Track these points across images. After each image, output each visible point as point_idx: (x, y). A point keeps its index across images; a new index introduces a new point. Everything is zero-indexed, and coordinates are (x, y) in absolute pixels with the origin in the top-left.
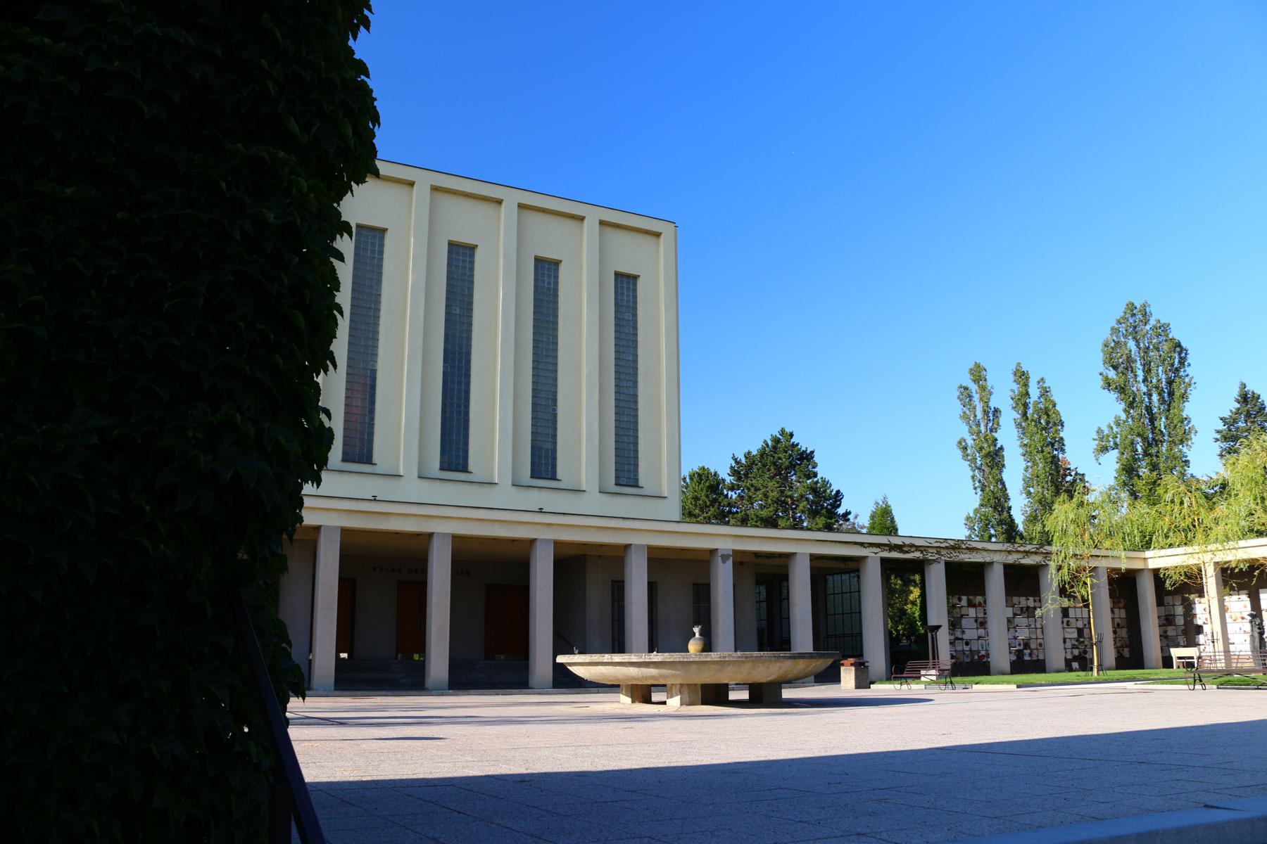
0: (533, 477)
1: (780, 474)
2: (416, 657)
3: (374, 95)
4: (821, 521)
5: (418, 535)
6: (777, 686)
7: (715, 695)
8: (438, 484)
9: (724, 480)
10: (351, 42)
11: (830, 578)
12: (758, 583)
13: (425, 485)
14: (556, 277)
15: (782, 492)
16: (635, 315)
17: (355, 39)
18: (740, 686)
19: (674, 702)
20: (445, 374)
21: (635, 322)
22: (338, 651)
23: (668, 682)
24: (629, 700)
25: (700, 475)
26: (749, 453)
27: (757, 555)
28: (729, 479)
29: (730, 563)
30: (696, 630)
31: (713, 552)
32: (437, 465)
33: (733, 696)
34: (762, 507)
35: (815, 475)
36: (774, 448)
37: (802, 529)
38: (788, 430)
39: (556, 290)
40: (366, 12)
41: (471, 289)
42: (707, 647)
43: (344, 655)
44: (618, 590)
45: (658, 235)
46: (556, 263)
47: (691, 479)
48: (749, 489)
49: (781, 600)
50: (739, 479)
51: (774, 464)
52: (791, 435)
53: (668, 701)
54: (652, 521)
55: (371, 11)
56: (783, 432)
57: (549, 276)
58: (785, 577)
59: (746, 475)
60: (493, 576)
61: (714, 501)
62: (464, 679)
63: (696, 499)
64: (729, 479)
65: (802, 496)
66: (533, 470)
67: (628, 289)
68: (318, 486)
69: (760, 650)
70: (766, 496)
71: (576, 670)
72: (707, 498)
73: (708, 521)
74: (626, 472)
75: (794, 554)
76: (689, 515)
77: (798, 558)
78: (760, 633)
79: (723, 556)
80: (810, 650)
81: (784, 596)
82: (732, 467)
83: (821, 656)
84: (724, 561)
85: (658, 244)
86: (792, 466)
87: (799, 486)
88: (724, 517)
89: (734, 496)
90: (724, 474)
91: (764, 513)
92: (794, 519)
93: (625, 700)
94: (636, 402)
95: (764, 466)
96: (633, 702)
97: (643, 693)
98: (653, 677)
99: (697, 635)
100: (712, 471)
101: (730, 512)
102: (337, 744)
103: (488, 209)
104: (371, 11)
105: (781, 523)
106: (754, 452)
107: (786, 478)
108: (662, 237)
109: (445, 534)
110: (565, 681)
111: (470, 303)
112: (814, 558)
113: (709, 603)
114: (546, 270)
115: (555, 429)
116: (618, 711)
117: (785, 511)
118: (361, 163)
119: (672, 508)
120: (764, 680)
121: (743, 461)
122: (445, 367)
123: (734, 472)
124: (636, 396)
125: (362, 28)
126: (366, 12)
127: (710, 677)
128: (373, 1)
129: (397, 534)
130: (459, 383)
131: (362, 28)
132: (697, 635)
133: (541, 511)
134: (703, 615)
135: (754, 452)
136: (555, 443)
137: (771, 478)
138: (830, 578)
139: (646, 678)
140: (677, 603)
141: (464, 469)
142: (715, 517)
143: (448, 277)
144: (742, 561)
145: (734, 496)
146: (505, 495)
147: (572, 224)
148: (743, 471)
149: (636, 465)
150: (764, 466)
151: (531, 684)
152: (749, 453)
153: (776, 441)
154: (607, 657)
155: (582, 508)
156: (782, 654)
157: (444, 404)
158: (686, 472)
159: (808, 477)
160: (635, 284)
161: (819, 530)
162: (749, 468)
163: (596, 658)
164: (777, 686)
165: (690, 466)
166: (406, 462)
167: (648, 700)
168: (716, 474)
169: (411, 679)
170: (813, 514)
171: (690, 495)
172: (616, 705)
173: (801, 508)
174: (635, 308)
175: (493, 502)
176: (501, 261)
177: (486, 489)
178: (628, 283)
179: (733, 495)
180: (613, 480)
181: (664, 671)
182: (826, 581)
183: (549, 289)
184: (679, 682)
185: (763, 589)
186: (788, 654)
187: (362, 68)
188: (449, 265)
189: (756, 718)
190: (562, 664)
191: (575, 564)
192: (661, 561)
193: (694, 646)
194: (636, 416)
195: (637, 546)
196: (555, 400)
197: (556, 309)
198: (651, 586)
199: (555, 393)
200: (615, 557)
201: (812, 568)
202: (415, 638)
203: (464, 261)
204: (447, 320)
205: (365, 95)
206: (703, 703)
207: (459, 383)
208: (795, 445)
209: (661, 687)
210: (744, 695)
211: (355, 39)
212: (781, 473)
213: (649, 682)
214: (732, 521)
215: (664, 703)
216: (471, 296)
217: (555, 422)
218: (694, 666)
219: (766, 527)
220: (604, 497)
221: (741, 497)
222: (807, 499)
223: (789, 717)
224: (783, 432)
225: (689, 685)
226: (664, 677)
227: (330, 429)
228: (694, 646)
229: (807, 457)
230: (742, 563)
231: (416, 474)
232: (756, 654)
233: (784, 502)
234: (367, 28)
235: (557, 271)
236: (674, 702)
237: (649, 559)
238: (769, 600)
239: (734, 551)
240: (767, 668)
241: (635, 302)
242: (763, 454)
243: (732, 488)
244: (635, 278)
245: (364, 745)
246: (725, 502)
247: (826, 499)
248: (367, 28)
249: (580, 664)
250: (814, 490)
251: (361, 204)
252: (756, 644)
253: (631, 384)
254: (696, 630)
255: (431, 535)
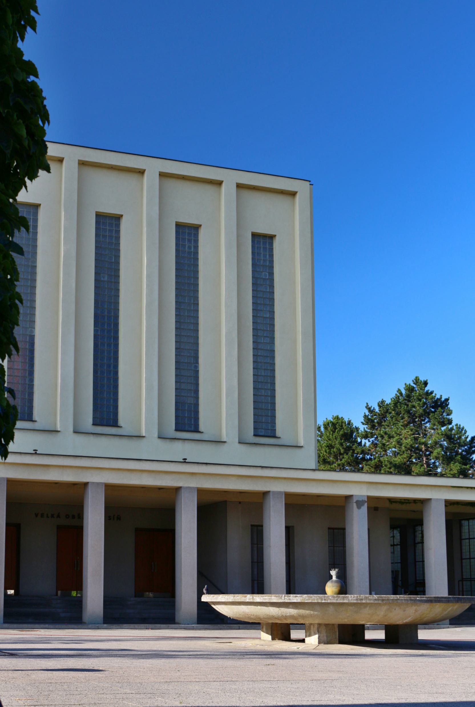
0: (177, 430)
1: (414, 422)
2: (74, 593)
3: (44, 94)
4: (455, 467)
5: (74, 484)
6: (412, 628)
7: (351, 634)
8: (92, 438)
9: (357, 429)
10: (20, 44)
11: (465, 523)
12: (393, 527)
13: (80, 439)
14: (196, 241)
15: (416, 439)
16: (272, 274)
17: (22, 40)
18: (375, 627)
19: (313, 640)
20: (96, 337)
21: (272, 280)
22: (6, 588)
23: (307, 622)
24: (269, 637)
25: (334, 424)
26: (383, 402)
27: (391, 501)
28: (362, 428)
29: (365, 509)
30: (333, 573)
31: (348, 498)
32: (90, 420)
33: (369, 635)
34: (395, 454)
35: (450, 422)
36: (408, 396)
37: (436, 475)
38: (422, 379)
39: (196, 253)
40: (33, 13)
41: (118, 257)
42: (343, 590)
43: (11, 592)
44: (257, 534)
45: (293, 194)
46: (196, 228)
47: (326, 428)
48: (382, 437)
49: (415, 544)
50: (373, 427)
51: (408, 412)
52: (426, 383)
53: (307, 640)
54: (293, 470)
55: (37, 13)
56: (417, 381)
57: (190, 241)
58: (420, 522)
59: (380, 424)
60: (143, 524)
61: (348, 449)
62: (115, 615)
63: (330, 447)
64: (362, 428)
65: (436, 443)
66: (177, 424)
67: (265, 249)
68: (5, 459)
69: (395, 593)
70: (399, 443)
71: (221, 609)
72: (341, 446)
73: (342, 469)
74: (264, 424)
75: (429, 500)
76: (324, 463)
77: (433, 504)
78: (395, 575)
79: (357, 502)
80: (446, 595)
81: (418, 539)
82: (365, 416)
83: (458, 600)
84: (359, 507)
85: (294, 204)
86: (426, 414)
87: (433, 434)
88: (358, 463)
89: (368, 444)
90: (358, 422)
91: (398, 460)
92: (428, 465)
93: (266, 637)
94: (273, 358)
95: (398, 414)
96: (273, 639)
97: (282, 631)
98: (292, 617)
99: (334, 578)
100: (346, 420)
101: (363, 459)
102: (11, 674)
103: (131, 180)
104: (37, 13)
105: (415, 469)
106: (388, 401)
107: (420, 426)
108: (298, 196)
109: (98, 484)
110: (209, 617)
111: (117, 270)
112: (449, 503)
113: (344, 546)
114: (187, 235)
115: (197, 385)
116: (259, 648)
117: (419, 458)
118: (35, 160)
119: (308, 457)
120: (400, 622)
121: (377, 410)
122: (95, 330)
123: (368, 421)
124: (273, 351)
125: (29, 29)
126: (33, 13)
127: (347, 618)
128: (39, 3)
129: (56, 483)
130: (109, 345)
131: (29, 29)
132: (334, 578)
133: (185, 461)
134: (338, 557)
135: (388, 401)
136: (197, 398)
137: (405, 426)
138: (465, 523)
139: (286, 617)
140: (314, 545)
141: (115, 424)
142: (349, 464)
143: (97, 248)
144: (377, 507)
145: (368, 444)
146: (152, 447)
147: (210, 189)
148: (376, 419)
149: (274, 417)
150: (398, 414)
151: (177, 620)
152: (383, 402)
153: (410, 389)
154: (249, 598)
155: (223, 459)
156: (418, 597)
157: (95, 365)
158: (320, 422)
159: (443, 424)
160: (271, 244)
161: (454, 476)
162: (383, 416)
163: (239, 598)
164: (412, 628)
165: (324, 416)
166: (63, 421)
167: (287, 638)
168: (349, 423)
169: (72, 615)
170: (448, 460)
171: (324, 444)
172: (257, 642)
173: (435, 454)
174: (272, 267)
175: (142, 455)
176: (145, 229)
177: (297, 451)
178: (265, 243)
179: (367, 443)
180: (252, 432)
181: (302, 612)
182: (461, 526)
183: (189, 253)
184: (317, 621)
185: (397, 534)
186: (424, 598)
187: (30, 68)
188: (97, 235)
189: (393, 659)
190: (207, 604)
191: (213, 509)
192: (298, 507)
193: (331, 588)
194: (274, 370)
195: (273, 492)
196: (196, 358)
197: (196, 272)
198: (289, 530)
199: (197, 351)
200: (254, 504)
201: (447, 514)
202: (72, 574)
203: (111, 231)
204: (96, 287)
205: (34, 94)
206: (341, 642)
207: (109, 345)
208: (429, 394)
209: (300, 626)
210: (381, 635)
211: (22, 40)
212: (415, 420)
213: (289, 621)
214: (366, 468)
215: (303, 641)
216: (118, 263)
217: (197, 378)
218: (331, 608)
219: (399, 473)
220: (243, 447)
221: (375, 445)
222: (441, 446)
223: (425, 659)
224: (417, 381)
225: (326, 625)
226: (303, 617)
227: (14, 408)
228: (331, 588)
229: (442, 405)
230: (376, 509)
231: (71, 430)
232: (392, 597)
233: (417, 449)
234: (34, 29)
235: (196, 235)
236: (313, 640)
237: (286, 505)
238: (403, 544)
239: (368, 497)
240: (403, 610)
241: (272, 262)
242: (396, 402)
243: (366, 436)
244: (272, 237)
245: (35, 675)
246: (359, 450)
247: (460, 446)
248: (34, 29)
249: (224, 604)
250: (449, 437)
251: (31, 192)
252: (390, 586)
253: (268, 340)
254: (333, 573)
255: (86, 484)
